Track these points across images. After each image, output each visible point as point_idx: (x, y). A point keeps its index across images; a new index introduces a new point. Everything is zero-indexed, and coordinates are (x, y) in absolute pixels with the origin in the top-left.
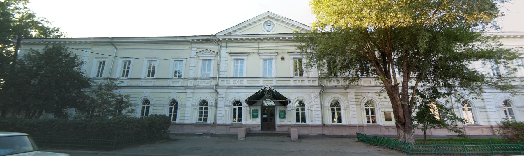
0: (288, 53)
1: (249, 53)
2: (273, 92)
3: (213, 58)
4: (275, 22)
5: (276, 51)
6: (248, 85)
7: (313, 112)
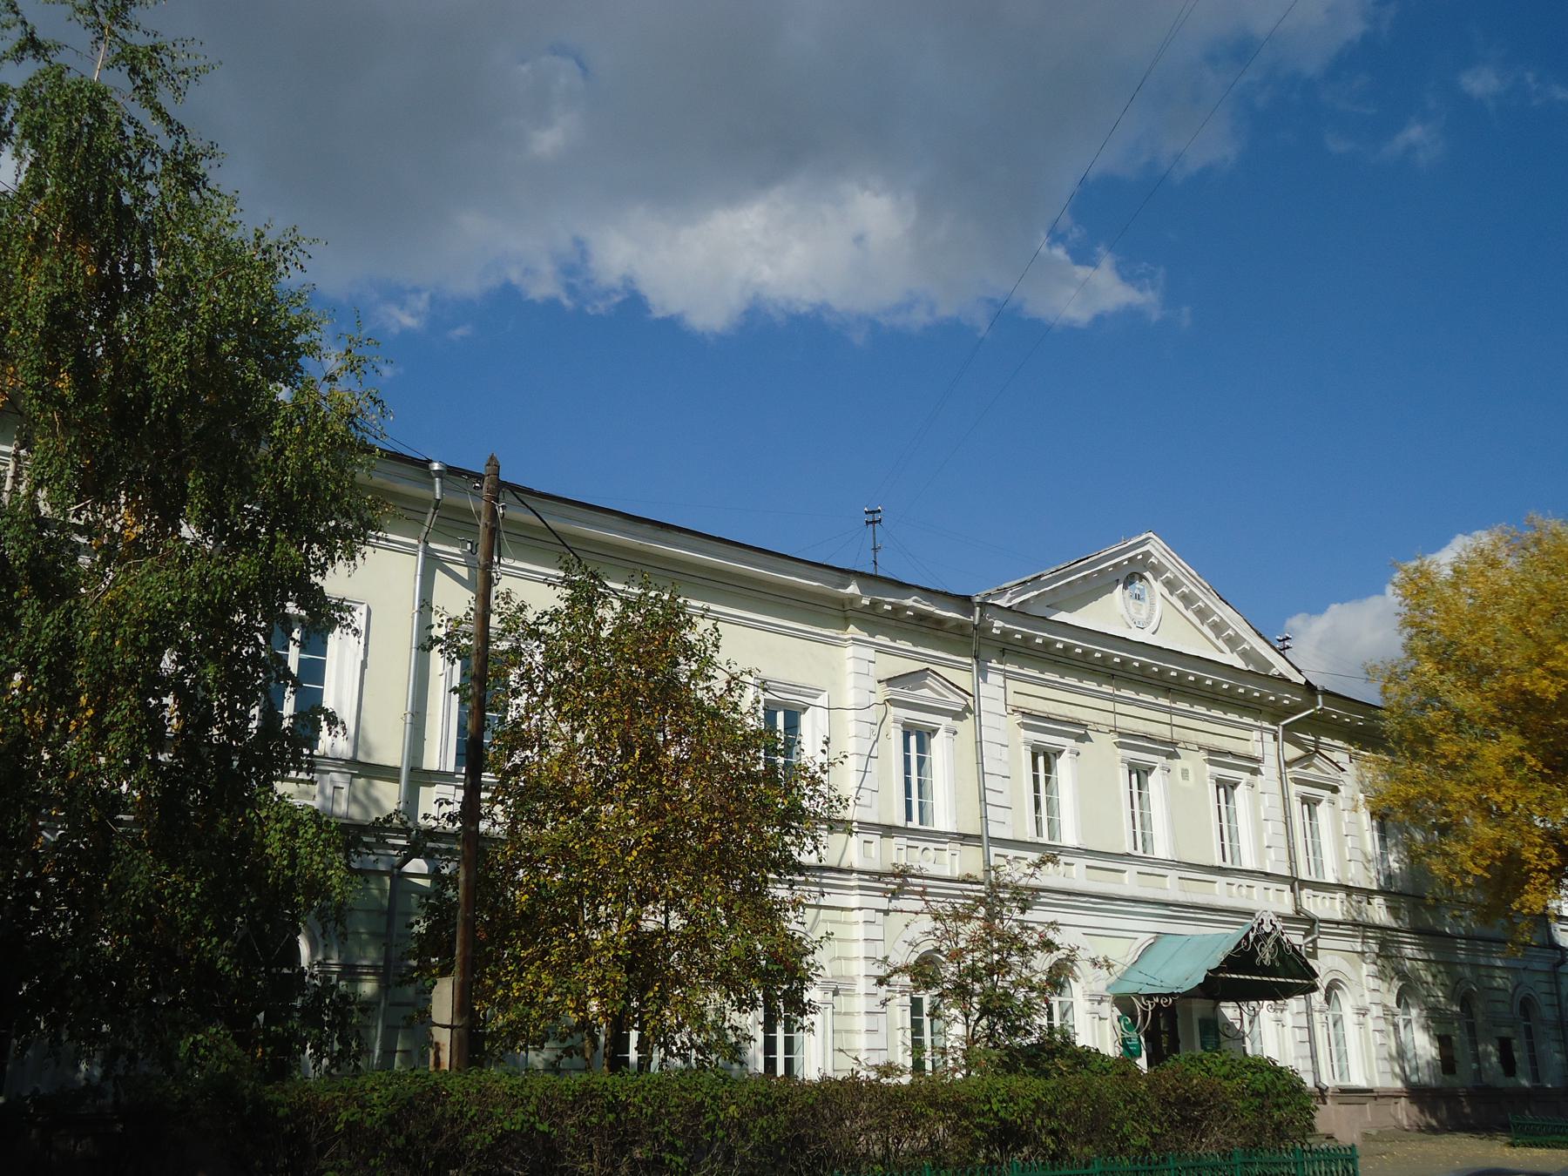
0: (1211, 752)
1: (1174, 744)
2: (1278, 940)
3: (945, 721)
4: (1158, 587)
5: (1163, 732)
6: (1181, 897)
7: (1288, 1029)
